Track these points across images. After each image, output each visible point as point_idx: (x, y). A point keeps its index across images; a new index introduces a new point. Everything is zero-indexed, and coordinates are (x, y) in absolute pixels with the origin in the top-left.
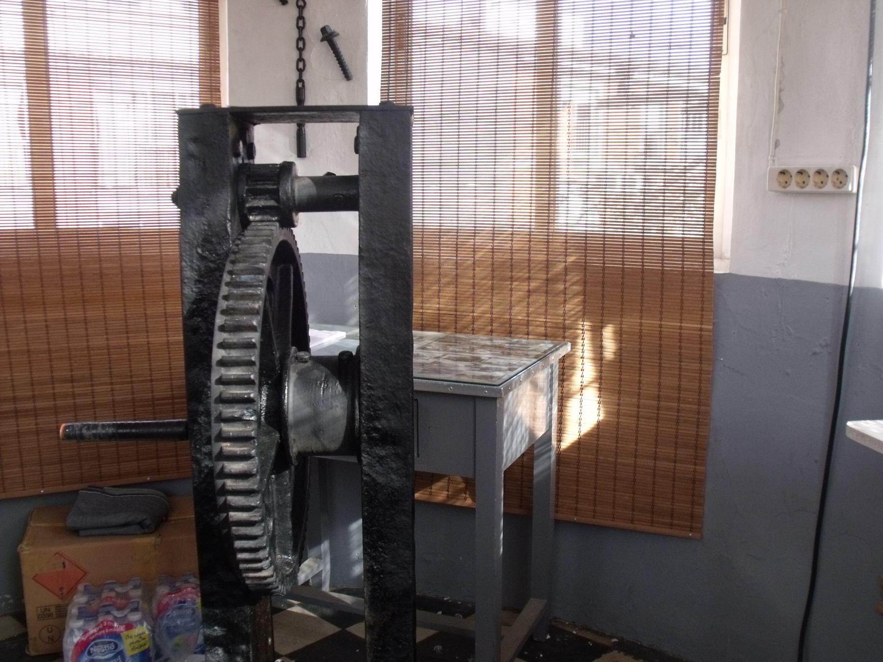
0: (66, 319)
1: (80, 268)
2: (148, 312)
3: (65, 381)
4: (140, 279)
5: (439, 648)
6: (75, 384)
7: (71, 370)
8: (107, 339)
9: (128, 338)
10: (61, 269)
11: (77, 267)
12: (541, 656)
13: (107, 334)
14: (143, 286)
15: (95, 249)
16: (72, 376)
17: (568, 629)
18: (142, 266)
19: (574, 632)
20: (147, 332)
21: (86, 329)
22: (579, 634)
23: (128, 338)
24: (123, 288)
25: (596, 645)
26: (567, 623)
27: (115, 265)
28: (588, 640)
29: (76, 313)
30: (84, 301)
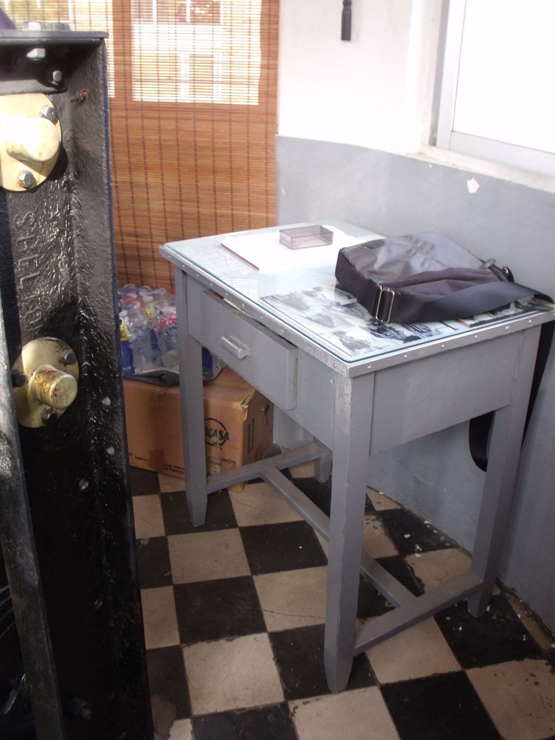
0: (131, 183)
1: (143, 138)
2: (199, 184)
3: (130, 235)
4: (194, 152)
5: (93, 441)
6: (139, 239)
7: (135, 227)
8: (164, 205)
9: (181, 206)
10: (128, 137)
11: (141, 137)
12: (460, 629)
13: (164, 200)
14: (231, 177)
15: (191, 139)
16: (136, 232)
17: (516, 608)
18: (195, 140)
19: (519, 616)
20: (198, 202)
21: (148, 193)
22: (523, 621)
23: (181, 206)
24: (178, 160)
25: (531, 640)
26: (521, 601)
27: (172, 138)
28: (525, 632)
29: (139, 178)
30: (146, 169)
